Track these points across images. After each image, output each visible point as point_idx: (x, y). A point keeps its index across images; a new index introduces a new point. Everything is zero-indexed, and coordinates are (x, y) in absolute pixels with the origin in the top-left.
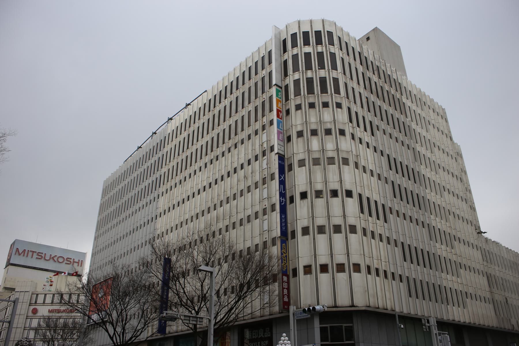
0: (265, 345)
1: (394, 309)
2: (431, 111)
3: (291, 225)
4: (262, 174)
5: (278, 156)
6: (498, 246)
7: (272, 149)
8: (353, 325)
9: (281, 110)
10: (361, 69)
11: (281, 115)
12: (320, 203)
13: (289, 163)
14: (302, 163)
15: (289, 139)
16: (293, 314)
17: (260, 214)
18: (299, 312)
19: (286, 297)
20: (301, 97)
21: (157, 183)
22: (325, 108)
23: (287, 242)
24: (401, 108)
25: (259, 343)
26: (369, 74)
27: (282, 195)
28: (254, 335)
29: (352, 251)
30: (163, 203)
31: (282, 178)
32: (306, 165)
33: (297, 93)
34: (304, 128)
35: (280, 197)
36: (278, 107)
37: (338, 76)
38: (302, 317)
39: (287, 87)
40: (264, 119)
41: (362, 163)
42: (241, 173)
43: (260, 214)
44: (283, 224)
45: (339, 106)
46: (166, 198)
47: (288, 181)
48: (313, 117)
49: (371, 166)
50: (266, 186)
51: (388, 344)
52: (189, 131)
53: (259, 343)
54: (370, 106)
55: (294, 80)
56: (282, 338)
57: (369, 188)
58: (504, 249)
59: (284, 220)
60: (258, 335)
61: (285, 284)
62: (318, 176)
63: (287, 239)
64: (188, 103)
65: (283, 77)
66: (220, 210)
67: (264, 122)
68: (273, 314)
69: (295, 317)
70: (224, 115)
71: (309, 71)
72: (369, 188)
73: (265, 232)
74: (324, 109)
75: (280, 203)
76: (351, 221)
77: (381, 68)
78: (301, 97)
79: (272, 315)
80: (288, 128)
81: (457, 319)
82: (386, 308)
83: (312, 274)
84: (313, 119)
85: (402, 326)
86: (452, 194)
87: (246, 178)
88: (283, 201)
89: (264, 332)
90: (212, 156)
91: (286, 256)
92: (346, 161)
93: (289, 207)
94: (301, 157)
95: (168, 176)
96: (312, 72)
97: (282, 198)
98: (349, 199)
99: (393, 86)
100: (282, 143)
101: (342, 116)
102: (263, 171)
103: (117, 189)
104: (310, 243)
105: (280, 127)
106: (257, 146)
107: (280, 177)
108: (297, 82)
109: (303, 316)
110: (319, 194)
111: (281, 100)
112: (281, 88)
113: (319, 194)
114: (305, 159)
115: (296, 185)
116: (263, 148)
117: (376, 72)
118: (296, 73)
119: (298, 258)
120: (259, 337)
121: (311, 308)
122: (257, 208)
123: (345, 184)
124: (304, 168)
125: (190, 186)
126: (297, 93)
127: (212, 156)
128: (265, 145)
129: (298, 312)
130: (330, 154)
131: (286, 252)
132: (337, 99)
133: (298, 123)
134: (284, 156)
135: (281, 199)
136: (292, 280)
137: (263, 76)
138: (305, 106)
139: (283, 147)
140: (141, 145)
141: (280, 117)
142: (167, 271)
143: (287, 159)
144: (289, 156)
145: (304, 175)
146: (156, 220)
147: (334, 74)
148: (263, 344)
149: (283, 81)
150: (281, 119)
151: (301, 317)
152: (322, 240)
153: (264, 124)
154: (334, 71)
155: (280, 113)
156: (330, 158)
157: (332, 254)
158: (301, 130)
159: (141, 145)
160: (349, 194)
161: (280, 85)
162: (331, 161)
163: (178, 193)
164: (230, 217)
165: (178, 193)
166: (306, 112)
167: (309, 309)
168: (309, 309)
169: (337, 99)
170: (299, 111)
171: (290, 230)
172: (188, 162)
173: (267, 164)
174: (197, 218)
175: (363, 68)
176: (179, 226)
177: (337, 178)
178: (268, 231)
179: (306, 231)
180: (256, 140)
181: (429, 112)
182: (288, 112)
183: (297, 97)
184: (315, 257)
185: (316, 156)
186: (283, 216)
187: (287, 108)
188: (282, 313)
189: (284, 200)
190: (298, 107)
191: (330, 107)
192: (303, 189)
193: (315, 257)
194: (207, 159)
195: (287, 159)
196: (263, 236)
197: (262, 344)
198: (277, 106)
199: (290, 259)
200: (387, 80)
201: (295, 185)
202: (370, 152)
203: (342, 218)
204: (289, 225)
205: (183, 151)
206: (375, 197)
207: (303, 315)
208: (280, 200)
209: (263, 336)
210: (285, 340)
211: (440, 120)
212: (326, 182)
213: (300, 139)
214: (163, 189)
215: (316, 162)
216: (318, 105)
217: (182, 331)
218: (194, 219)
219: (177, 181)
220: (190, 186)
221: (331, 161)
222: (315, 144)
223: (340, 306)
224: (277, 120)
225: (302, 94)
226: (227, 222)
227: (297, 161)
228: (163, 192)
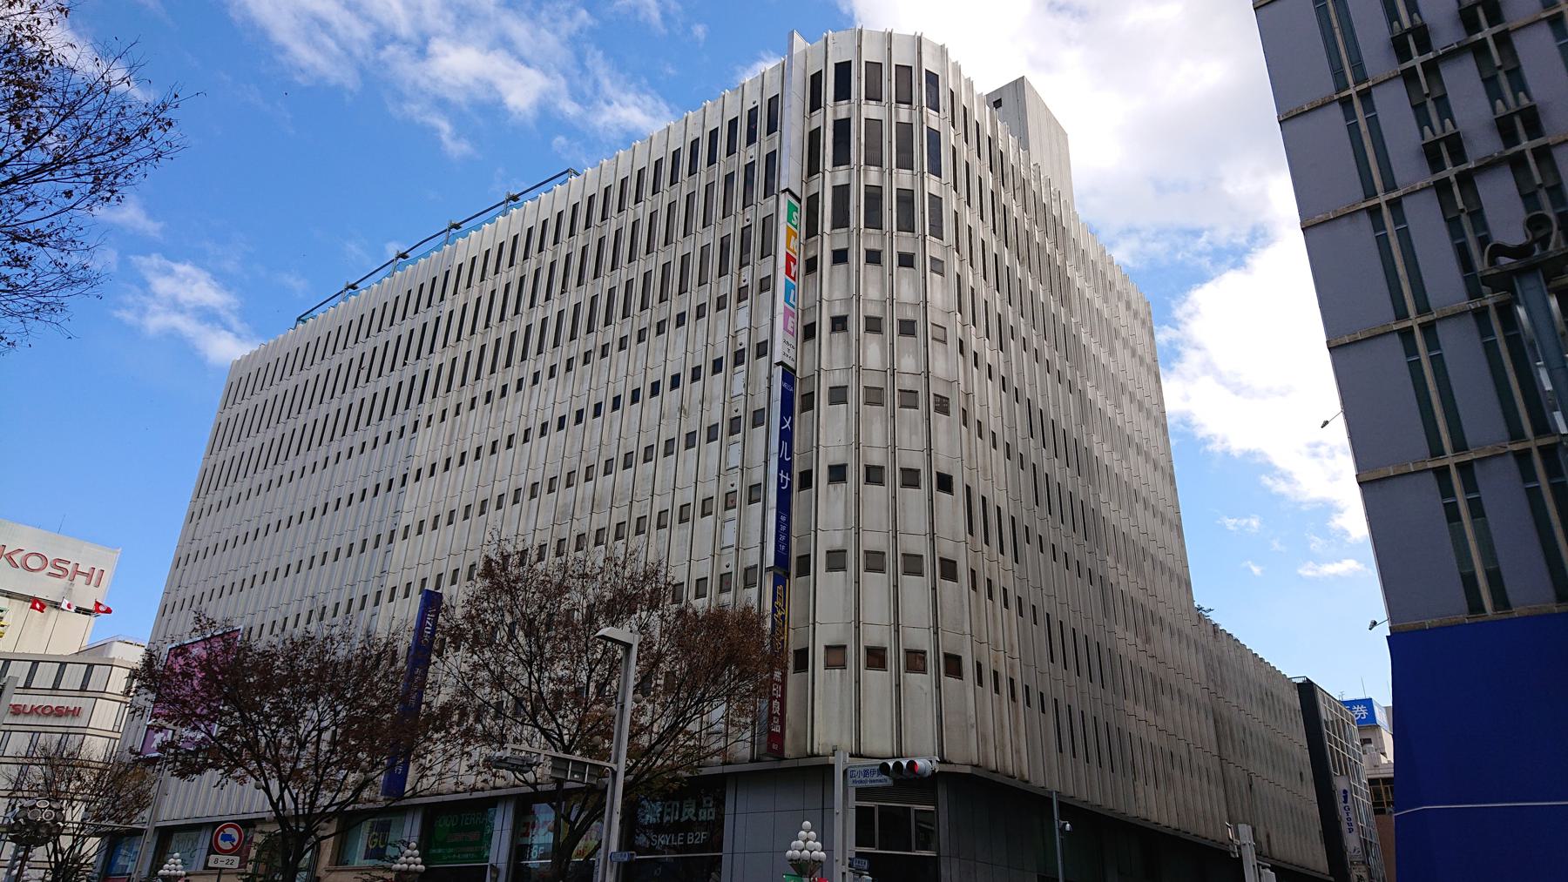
0: (696, 842)
1: (1027, 777)
2: (1122, 306)
3: (798, 541)
4: (731, 407)
5: (783, 369)
6: (1238, 647)
7: (762, 349)
8: (937, 808)
9: (796, 257)
10: (989, 183)
11: (794, 269)
12: (876, 495)
13: (807, 390)
14: (838, 395)
15: (810, 332)
16: (845, 772)
17: (718, 504)
18: (862, 769)
19: (776, 721)
20: (848, 231)
21: (418, 389)
22: (906, 269)
23: (787, 581)
24: (1061, 287)
25: (681, 836)
26: (1005, 197)
27: (785, 466)
28: (669, 814)
29: (945, 622)
30: (428, 445)
31: (788, 425)
32: (849, 402)
33: (841, 219)
34: (849, 308)
35: (779, 472)
36: (789, 249)
37: (941, 192)
38: (869, 784)
39: (813, 201)
40: (743, 274)
41: (976, 413)
42: (670, 397)
43: (718, 504)
44: (783, 538)
45: (938, 266)
46: (438, 435)
47: (799, 434)
48: (872, 284)
49: (993, 424)
50: (739, 437)
51: (1009, 867)
52: (523, 269)
53: (681, 836)
54: (1001, 279)
55: (834, 187)
56: (802, 833)
57: (985, 474)
58: (1250, 657)
59: (783, 528)
60: (680, 816)
61: (775, 687)
62: (875, 432)
63: (788, 575)
64: (511, 194)
65: (805, 173)
66: (604, 483)
67: (744, 281)
68: (733, 761)
69: (850, 781)
70: (632, 244)
71: (872, 168)
72: (985, 474)
73: (726, 551)
74: (902, 269)
75: (780, 485)
76: (946, 549)
77: (1030, 184)
78: (848, 231)
79: (730, 763)
80: (809, 303)
81: (1154, 817)
82: (1011, 773)
83: (845, 668)
84: (873, 292)
85: (1068, 825)
86: (1064, 491)
87: (685, 413)
88: (784, 479)
89: (699, 806)
90: (584, 343)
91: (783, 617)
92: (943, 406)
93: (797, 497)
94: (838, 379)
95: (448, 378)
96: (882, 173)
97: (785, 474)
98: (944, 496)
99: (1051, 233)
100: (791, 340)
101: (939, 293)
102: (733, 400)
103: (279, 389)
104: (846, 591)
105: (791, 301)
106: (721, 337)
107: (782, 423)
108: (841, 193)
109: (871, 781)
110: (874, 475)
111: (797, 232)
112: (799, 201)
113: (874, 475)
114: (847, 387)
115: (821, 447)
116: (736, 344)
117: (1019, 194)
118: (841, 168)
119: (814, 624)
120: (682, 820)
121: (904, 763)
122: (709, 489)
123: (936, 460)
124: (842, 406)
125: (515, 412)
126: (841, 219)
127: (584, 343)
128: (743, 338)
129: (857, 769)
130: (907, 383)
131: (784, 607)
132: (934, 248)
133: (834, 297)
134: (795, 372)
135: (782, 475)
136: (792, 678)
137: (749, 161)
138: (857, 258)
139: (794, 351)
140: (358, 282)
141: (793, 275)
142: (430, 621)
143: (801, 380)
144: (807, 373)
145: (842, 424)
146: (404, 488)
147: (932, 185)
148: (692, 838)
149: (804, 184)
150: (794, 280)
151: (865, 782)
152: (876, 586)
153: (744, 284)
154: (932, 176)
155: (792, 264)
156: (905, 391)
157: (898, 625)
158: (843, 314)
159: (358, 282)
160: (945, 483)
161: (797, 192)
162: (909, 398)
163: (477, 426)
164: (631, 502)
165: (477, 426)
166: (858, 271)
167: (898, 765)
168: (898, 765)
169: (934, 248)
170: (842, 267)
171: (794, 554)
172: (514, 350)
173: (746, 386)
174: (533, 496)
175: (995, 179)
176: (475, 510)
177: (919, 442)
178: (737, 550)
179: (836, 560)
180: (719, 322)
181: (1117, 306)
182: (812, 265)
183: (837, 231)
184: (858, 627)
185: (875, 381)
186: (783, 518)
187: (811, 254)
188: (758, 760)
189: (787, 479)
190: (840, 257)
191: (917, 267)
192: (837, 458)
193: (858, 627)
194: (575, 349)
195: (801, 380)
196: (719, 560)
197: (689, 838)
198: (788, 247)
199: (791, 626)
200: (1041, 216)
201: (818, 445)
202: (993, 387)
203: (926, 538)
204: (794, 541)
205: (502, 319)
206: (999, 498)
207: (873, 779)
208: (779, 477)
209: (694, 819)
210: (808, 839)
211: (1138, 330)
212: (893, 448)
213: (839, 337)
214: (432, 407)
215: (874, 397)
216: (890, 259)
217: (1291, 864)
218: (525, 495)
219: (481, 392)
220: (515, 412)
221: (909, 398)
222: (873, 352)
223: (868, 755)
224: (786, 280)
225: (853, 224)
226: (619, 515)
227: (828, 389)
228: (363, 400)
